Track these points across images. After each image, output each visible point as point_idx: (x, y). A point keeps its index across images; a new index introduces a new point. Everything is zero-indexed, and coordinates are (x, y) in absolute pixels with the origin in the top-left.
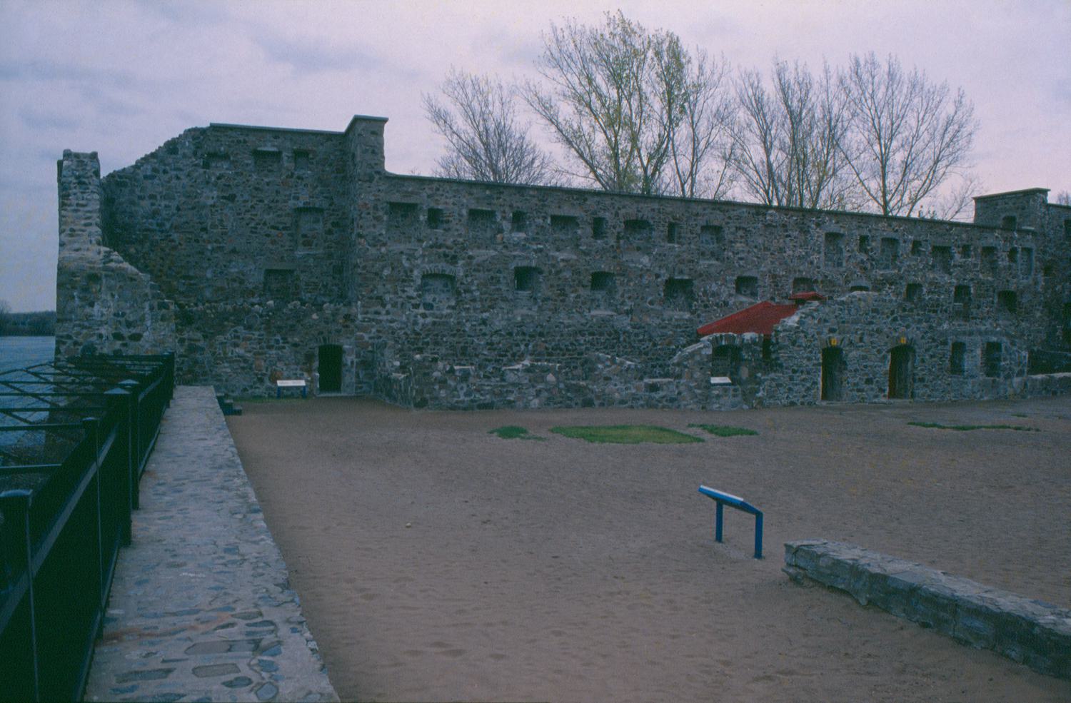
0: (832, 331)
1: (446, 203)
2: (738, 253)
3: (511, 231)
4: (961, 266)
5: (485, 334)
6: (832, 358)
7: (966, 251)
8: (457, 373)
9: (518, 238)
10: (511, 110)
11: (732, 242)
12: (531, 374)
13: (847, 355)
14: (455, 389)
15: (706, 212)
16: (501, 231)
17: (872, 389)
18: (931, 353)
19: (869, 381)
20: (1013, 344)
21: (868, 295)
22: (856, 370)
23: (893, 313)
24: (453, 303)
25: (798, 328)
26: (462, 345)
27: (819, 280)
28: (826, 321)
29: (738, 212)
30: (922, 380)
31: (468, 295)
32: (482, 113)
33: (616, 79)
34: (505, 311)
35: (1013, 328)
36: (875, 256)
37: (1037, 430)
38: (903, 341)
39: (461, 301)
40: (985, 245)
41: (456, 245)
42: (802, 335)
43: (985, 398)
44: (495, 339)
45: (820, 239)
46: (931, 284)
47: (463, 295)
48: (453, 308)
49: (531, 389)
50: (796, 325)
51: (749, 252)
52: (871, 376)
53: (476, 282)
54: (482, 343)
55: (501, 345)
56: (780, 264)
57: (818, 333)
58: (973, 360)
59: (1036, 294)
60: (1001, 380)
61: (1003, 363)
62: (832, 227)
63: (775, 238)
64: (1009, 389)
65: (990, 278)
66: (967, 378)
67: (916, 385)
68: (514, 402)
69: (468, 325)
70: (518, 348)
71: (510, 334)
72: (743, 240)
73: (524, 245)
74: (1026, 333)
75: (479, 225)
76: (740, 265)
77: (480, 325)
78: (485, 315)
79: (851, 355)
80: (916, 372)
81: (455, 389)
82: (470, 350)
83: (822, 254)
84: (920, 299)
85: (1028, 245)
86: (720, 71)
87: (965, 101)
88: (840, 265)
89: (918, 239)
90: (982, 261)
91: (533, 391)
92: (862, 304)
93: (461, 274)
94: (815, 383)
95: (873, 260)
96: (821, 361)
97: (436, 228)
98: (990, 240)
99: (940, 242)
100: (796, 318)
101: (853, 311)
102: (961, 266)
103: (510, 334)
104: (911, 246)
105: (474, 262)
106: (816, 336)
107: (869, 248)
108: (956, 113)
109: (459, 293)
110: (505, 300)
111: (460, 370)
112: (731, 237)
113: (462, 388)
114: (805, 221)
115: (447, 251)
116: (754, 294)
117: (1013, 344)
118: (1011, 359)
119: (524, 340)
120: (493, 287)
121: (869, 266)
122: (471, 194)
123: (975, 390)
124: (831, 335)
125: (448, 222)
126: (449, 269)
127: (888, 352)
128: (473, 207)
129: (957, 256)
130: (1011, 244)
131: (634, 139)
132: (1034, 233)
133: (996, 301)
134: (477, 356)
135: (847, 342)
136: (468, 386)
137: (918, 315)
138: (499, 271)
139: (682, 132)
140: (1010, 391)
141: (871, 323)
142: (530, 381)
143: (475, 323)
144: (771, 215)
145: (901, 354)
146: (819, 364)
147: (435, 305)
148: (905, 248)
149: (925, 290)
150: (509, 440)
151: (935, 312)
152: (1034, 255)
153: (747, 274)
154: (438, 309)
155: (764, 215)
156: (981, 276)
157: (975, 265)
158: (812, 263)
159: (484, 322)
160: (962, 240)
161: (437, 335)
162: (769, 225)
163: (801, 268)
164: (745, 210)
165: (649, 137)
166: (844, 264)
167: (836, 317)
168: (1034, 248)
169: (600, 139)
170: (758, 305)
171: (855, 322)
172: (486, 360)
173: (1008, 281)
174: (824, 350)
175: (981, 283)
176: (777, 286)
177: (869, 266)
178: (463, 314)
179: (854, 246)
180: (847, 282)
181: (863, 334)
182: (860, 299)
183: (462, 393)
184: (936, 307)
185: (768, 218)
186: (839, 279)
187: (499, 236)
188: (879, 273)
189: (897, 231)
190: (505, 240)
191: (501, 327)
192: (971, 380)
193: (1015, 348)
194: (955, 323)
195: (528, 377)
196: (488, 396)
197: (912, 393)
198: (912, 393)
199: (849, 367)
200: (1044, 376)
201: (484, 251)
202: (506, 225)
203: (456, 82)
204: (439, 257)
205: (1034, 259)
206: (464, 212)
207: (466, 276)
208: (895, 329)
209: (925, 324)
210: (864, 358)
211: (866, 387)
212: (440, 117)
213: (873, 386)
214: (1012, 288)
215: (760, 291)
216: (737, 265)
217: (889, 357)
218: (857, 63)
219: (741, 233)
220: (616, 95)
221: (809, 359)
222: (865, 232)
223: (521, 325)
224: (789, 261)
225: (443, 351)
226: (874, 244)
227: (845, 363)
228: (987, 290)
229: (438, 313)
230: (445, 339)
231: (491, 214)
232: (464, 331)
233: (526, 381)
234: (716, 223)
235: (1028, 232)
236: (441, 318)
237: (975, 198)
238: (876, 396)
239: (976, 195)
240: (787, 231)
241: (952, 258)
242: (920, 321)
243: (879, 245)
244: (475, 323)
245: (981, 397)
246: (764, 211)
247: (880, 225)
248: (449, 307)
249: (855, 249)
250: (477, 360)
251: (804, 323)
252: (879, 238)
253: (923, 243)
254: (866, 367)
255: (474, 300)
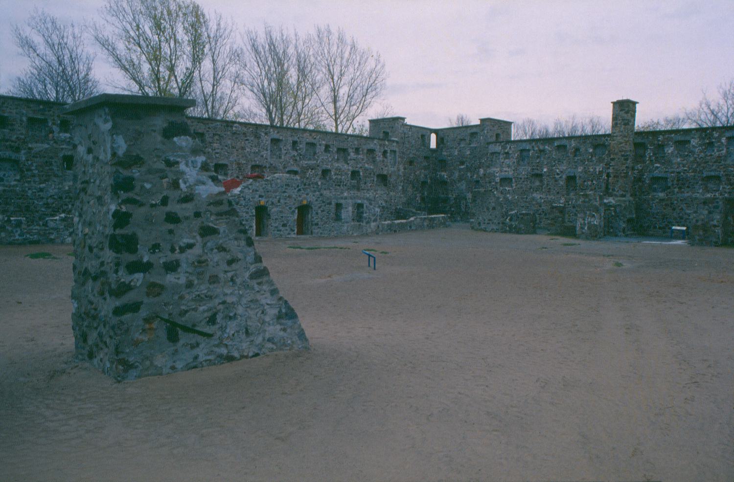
0: (261, 196)
1: (11, 112)
2: (215, 150)
3: (59, 133)
4: (354, 160)
5: (42, 198)
6: (261, 212)
7: (357, 151)
8: (13, 222)
9: (65, 137)
10: (81, 43)
11: (210, 143)
12: (65, 223)
13: (270, 210)
14: (12, 232)
15: (193, 124)
16: (52, 132)
17: (287, 230)
18: (321, 209)
19: (284, 225)
20: (371, 204)
21: (283, 176)
22: (276, 219)
23: (298, 186)
24: (18, 177)
25: (239, 195)
26: (26, 205)
27: (267, 166)
28: (257, 191)
29: (214, 125)
30: (317, 224)
31: (29, 173)
32: (60, 44)
33: (158, 27)
34: (57, 183)
35: (385, 195)
36: (302, 153)
37: (349, 249)
38: (305, 202)
39: (24, 176)
40: (369, 148)
41: (19, 140)
42: (242, 199)
43: (355, 235)
44: (50, 201)
45: (267, 142)
46: (336, 169)
47: (26, 172)
48: (19, 181)
49: (65, 232)
50: (239, 193)
51: (222, 149)
52: (285, 222)
53: (34, 164)
54: (41, 203)
55: (54, 205)
56: (243, 157)
57: (252, 198)
58: (348, 213)
59: (399, 176)
60: (364, 224)
61: (365, 215)
62: (275, 135)
63: (239, 141)
64: (368, 229)
65: (372, 167)
66: (343, 223)
67: (313, 227)
68: (54, 239)
69: (30, 192)
70: (66, 207)
71: (61, 198)
72: (218, 142)
73: (69, 142)
74: (393, 198)
75: (36, 127)
76: (216, 157)
77: (38, 192)
78: (42, 186)
79: (273, 210)
80: (312, 220)
81: (12, 232)
82: (32, 207)
83: (269, 151)
84: (331, 179)
85: (394, 149)
86: (230, 28)
87: (382, 59)
88: (280, 158)
89: (328, 143)
90: (367, 157)
91: (67, 233)
92: (279, 181)
93: (24, 159)
94: (251, 227)
95: (301, 155)
96: (254, 214)
97: (4, 128)
98: (371, 146)
99: (342, 146)
100: (239, 189)
101: (274, 185)
102: (354, 160)
103: (61, 198)
104: (324, 148)
105: (33, 151)
106: (251, 199)
107: (298, 148)
108: (376, 66)
109: (22, 171)
110: (56, 176)
111: (15, 220)
112: (211, 140)
113: (17, 231)
114: (258, 131)
115: (13, 144)
116: (226, 174)
117: (371, 204)
118: (369, 212)
119: (71, 201)
120: (48, 168)
121: (298, 158)
122: (29, 107)
123: (349, 229)
124: (261, 199)
125: (12, 125)
126: (14, 156)
127: (296, 208)
128: (30, 115)
129: (352, 154)
130: (384, 148)
131: (172, 69)
132: (397, 142)
133: (375, 180)
134: (37, 212)
135: (270, 203)
136: (21, 230)
137: (313, 187)
138: (52, 158)
139: (207, 64)
140: (369, 230)
141: (285, 192)
142: (65, 227)
143: (35, 191)
144: (236, 127)
145: (303, 210)
146: (253, 216)
147: (5, 179)
148: (320, 149)
149: (333, 173)
150: (35, 260)
151: (339, 186)
152: (397, 154)
153: (221, 162)
154: (7, 181)
155: (232, 127)
156: (366, 165)
157: (363, 159)
158: (262, 156)
159: (41, 190)
160: (354, 145)
161: (7, 198)
162: (234, 133)
163: (256, 159)
164: (218, 123)
165: (181, 69)
166: (283, 157)
167: (263, 188)
168: (397, 150)
169: (146, 68)
170: (229, 181)
171: (275, 192)
172: (44, 214)
173: (382, 169)
174: (256, 208)
175: (366, 170)
176: (240, 169)
177: (298, 158)
178: (26, 185)
179: (289, 147)
180: (285, 168)
181: (280, 198)
182: (278, 179)
183: (17, 235)
184: (339, 183)
185: (234, 129)
186: (279, 166)
187: (51, 135)
188: (304, 163)
189: (315, 138)
190: (55, 138)
191: (54, 194)
192: (346, 225)
193: (372, 207)
194: (352, 192)
195: (63, 224)
196: (35, 236)
197: (311, 232)
198: (311, 232)
199: (272, 217)
200: (389, 222)
201: (40, 145)
202: (55, 128)
203: (39, 18)
204: (7, 148)
205: (397, 157)
206: (24, 119)
207: (28, 160)
208: (300, 196)
209: (318, 193)
210: (281, 212)
211: (283, 229)
212: (28, 45)
213: (287, 228)
214: (385, 173)
215: (230, 172)
216: (214, 157)
217: (297, 211)
218: (319, 31)
219: (217, 137)
220: (157, 39)
221: (247, 213)
222: (296, 139)
223: (68, 192)
224: (248, 155)
225: (12, 208)
226: (301, 146)
227: (269, 215)
228: (370, 174)
229: (7, 183)
230: (13, 201)
231: (44, 122)
232: (27, 196)
233: (63, 227)
234: (200, 131)
235: (394, 141)
236: (10, 187)
237: (612, 102)
238: (289, 234)
239: (370, 119)
240: (246, 137)
241: (349, 155)
242: (315, 191)
243: (305, 146)
244: (35, 191)
245: (352, 234)
246: (231, 124)
247: (305, 135)
248: (15, 180)
249: (290, 148)
250: (37, 214)
251: (243, 192)
252: (305, 143)
253: (331, 146)
254: (282, 217)
255: (34, 176)
